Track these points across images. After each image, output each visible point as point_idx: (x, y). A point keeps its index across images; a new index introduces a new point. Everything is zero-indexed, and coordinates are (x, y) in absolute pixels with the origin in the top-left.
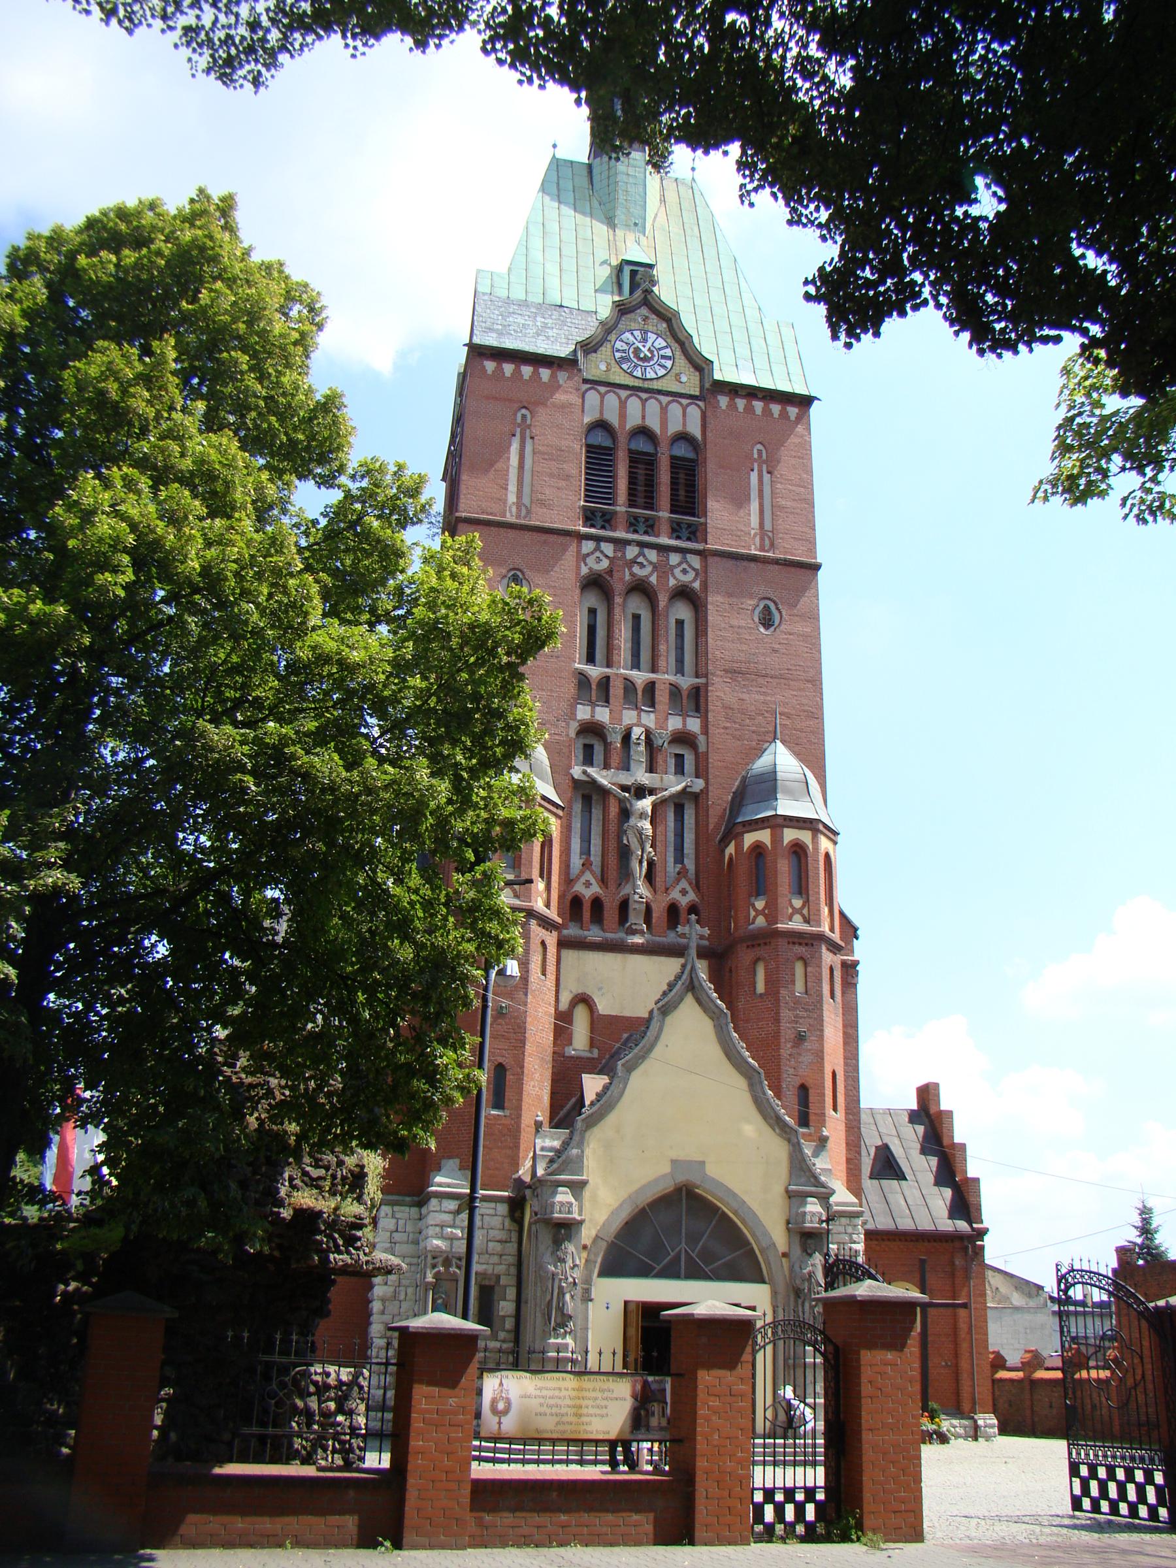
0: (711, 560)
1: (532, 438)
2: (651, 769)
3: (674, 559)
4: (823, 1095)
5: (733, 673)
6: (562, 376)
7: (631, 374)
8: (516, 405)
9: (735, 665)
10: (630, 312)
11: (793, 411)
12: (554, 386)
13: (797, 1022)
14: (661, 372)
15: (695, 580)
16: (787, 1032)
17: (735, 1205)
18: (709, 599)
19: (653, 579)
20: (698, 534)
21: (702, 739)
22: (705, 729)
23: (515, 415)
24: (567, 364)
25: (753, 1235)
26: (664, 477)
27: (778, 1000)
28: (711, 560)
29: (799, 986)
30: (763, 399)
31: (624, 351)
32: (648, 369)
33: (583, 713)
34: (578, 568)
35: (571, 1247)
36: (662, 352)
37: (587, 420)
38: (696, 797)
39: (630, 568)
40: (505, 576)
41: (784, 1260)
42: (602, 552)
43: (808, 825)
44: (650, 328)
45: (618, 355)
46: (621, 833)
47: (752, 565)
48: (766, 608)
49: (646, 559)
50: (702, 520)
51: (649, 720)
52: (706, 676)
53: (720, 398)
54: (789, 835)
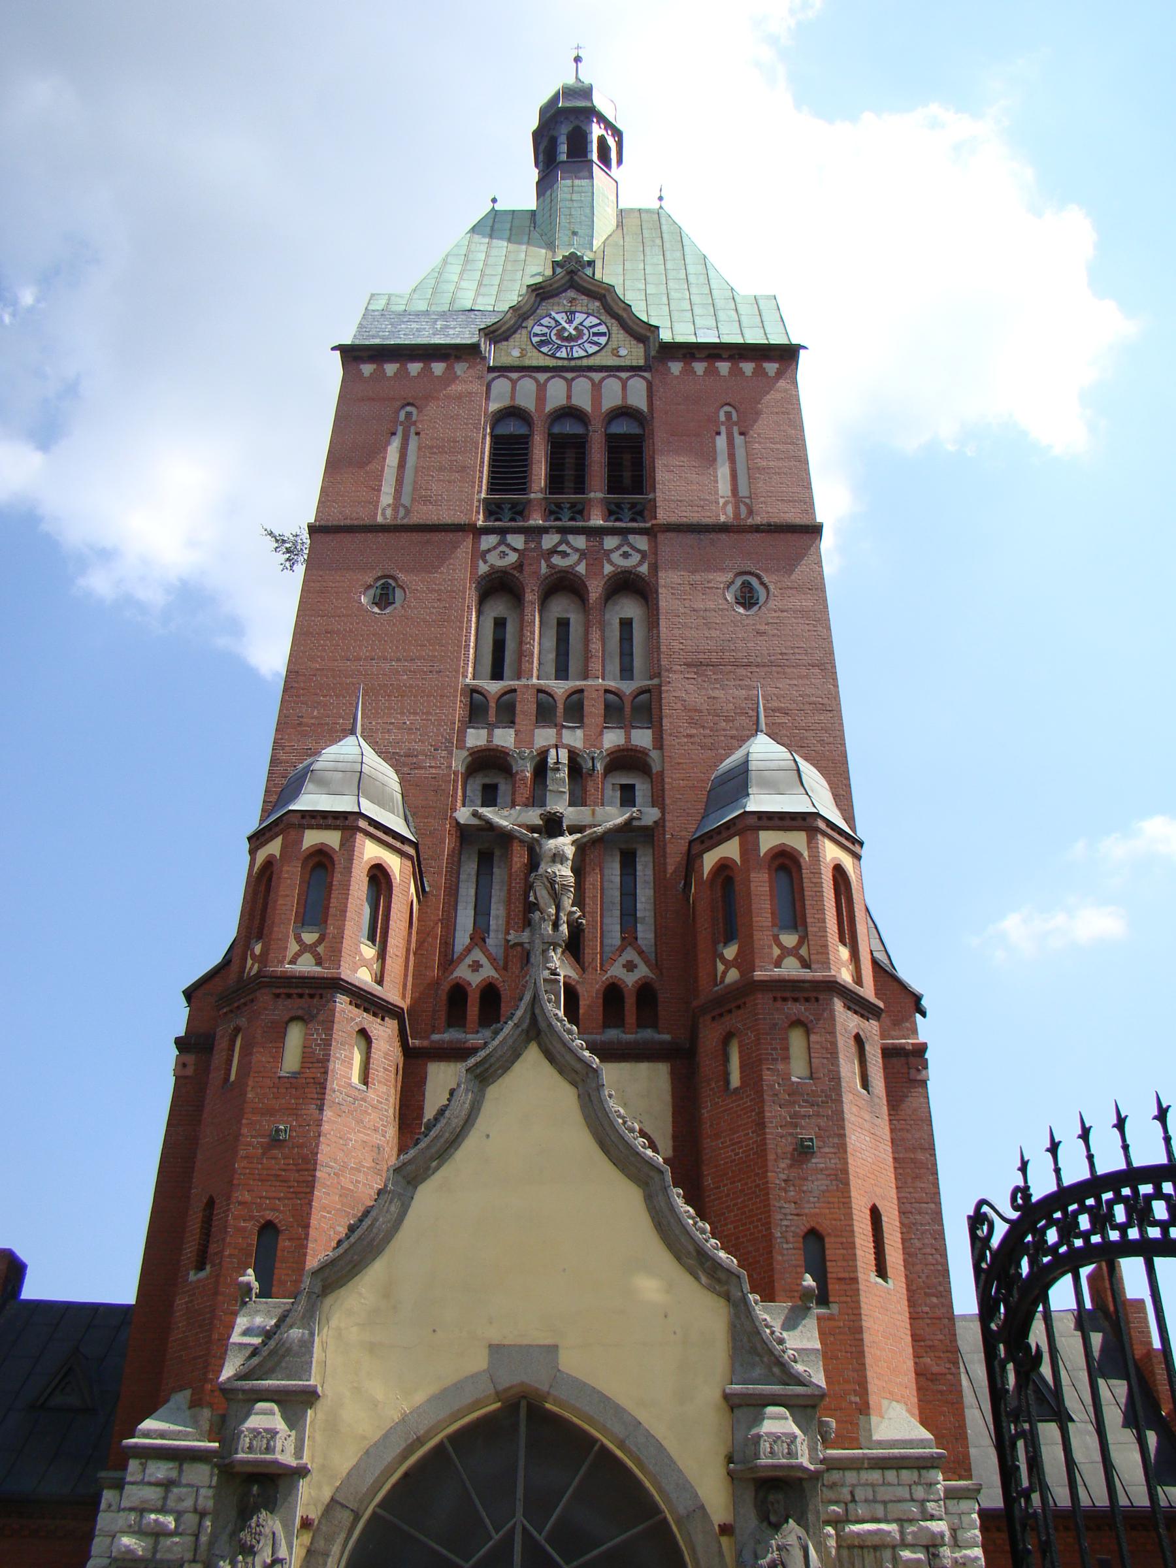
0: (661, 537)
1: (417, 434)
2: (576, 800)
3: (610, 542)
4: (852, 1246)
5: (698, 666)
6: (460, 368)
7: (553, 356)
8: (399, 403)
9: (701, 656)
10: (552, 296)
11: (771, 368)
12: (450, 378)
13: (796, 1126)
14: (592, 349)
15: (640, 563)
16: (778, 1140)
17: (618, 1429)
18: (661, 582)
19: (581, 569)
20: (646, 513)
21: (654, 754)
22: (659, 743)
23: (397, 412)
24: (469, 352)
25: (660, 1490)
26: (597, 456)
27: (760, 1093)
28: (661, 537)
29: (798, 1070)
30: (730, 358)
31: (543, 335)
32: (575, 349)
33: (476, 738)
34: (474, 567)
35: (271, 1523)
36: (595, 330)
37: (493, 407)
38: (650, 835)
39: (547, 560)
40: (370, 587)
41: (724, 1540)
42: (508, 545)
43: (799, 823)
44: (579, 309)
45: (537, 339)
46: (529, 887)
47: (723, 536)
48: (747, 586)
49: (571, 547)
50: (651, 496)
51: (575, 738)
52: (659, 675)
53: (670, 364)
54: (768, 840)
